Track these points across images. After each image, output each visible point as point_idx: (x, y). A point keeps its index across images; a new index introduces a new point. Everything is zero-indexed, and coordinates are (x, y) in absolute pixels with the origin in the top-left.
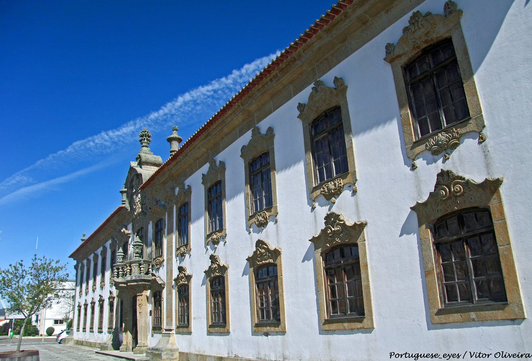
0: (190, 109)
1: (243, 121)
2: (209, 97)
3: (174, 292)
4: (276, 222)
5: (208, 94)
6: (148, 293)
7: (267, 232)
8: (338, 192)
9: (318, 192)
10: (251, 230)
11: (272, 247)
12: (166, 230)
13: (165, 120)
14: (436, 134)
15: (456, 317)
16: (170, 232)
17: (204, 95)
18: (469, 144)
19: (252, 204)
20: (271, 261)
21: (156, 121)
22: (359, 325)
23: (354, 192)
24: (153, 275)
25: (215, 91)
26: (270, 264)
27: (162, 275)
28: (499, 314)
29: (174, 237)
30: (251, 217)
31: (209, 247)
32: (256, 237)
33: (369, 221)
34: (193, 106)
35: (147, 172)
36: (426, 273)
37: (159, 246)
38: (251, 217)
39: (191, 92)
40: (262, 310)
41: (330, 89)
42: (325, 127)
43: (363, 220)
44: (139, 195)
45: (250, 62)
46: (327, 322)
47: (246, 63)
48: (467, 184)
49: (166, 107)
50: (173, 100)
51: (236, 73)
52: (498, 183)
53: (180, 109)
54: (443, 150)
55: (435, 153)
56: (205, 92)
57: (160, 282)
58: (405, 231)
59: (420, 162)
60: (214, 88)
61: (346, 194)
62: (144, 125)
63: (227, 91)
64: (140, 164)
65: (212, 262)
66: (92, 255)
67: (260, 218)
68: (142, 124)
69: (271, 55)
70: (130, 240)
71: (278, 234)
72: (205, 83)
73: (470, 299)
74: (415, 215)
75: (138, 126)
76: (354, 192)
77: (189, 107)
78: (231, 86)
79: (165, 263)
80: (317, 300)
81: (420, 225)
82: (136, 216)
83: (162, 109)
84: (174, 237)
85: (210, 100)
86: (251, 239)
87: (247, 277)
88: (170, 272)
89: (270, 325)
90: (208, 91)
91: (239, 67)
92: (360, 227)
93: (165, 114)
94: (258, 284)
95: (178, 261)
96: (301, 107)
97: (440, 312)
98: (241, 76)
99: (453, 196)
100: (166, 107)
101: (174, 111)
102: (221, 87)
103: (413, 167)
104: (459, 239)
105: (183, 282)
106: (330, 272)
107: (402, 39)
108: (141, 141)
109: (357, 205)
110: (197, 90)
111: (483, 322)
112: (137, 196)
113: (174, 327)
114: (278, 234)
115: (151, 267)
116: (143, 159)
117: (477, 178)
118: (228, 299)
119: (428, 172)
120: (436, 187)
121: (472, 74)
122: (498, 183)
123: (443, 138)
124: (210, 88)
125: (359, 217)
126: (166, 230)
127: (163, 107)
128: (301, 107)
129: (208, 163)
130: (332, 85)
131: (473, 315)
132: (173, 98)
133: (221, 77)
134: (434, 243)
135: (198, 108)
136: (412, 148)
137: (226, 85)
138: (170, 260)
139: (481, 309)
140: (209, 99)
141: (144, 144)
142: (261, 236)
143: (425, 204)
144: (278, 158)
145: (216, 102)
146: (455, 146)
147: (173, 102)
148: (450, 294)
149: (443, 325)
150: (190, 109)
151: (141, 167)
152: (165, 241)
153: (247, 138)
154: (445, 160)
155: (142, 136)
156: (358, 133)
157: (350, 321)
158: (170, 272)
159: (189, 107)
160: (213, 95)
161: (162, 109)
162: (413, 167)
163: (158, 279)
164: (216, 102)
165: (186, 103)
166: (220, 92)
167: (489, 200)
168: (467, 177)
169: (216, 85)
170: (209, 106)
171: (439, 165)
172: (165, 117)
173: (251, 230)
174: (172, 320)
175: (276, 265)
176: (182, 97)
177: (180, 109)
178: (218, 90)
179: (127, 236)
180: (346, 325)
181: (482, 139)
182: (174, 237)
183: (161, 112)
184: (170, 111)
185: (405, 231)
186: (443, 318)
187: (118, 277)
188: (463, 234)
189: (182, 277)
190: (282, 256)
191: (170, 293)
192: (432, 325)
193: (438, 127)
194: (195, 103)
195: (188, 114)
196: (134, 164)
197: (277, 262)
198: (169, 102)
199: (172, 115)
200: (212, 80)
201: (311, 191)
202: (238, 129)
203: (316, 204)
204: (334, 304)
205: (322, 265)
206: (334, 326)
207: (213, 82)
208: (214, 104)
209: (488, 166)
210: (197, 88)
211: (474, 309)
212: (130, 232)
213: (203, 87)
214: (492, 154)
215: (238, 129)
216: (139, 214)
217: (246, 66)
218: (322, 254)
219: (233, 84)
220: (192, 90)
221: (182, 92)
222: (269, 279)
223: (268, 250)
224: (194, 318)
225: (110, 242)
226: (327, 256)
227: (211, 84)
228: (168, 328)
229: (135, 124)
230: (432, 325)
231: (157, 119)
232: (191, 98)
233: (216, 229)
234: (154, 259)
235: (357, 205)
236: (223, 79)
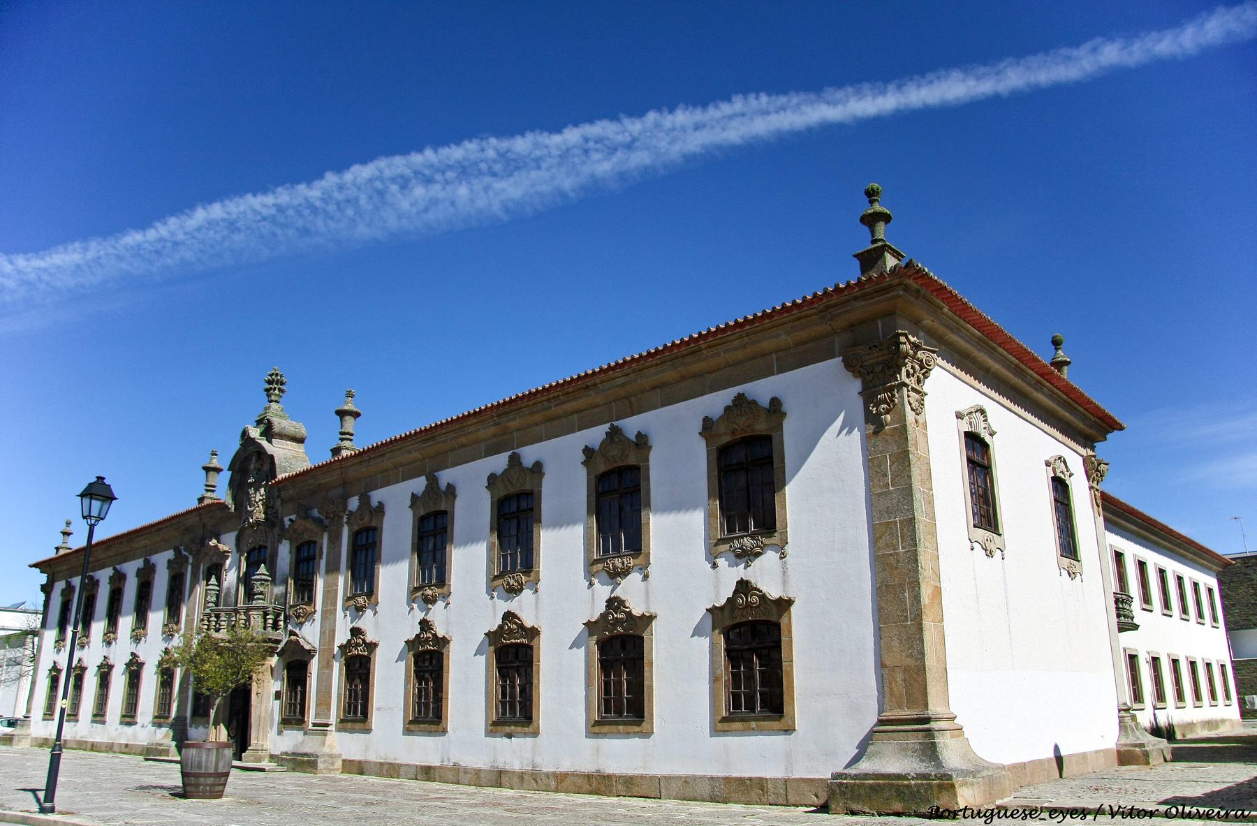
0: (218, 237)
1: (495, 436)
2: (264, 219)
3: (337, 668)
4: (536, 591)
5: (265, 212)
6: (274, 660)
7: (520, 601)
8: (625, 573)
9: (600, 566)
10: (495, 594)
11: (528, 623)
12: (323, 563)
13: (158, 252)
14: (742, 537)
15: (738, 725)
16: (333, 569)
17: (254, 211)
18: (770, 557)
19: (499, 559)
20: (525, 641)
21: (137, 250)
22: (637, 729)
23: (646, 577)
24: (292, 633)
25: (281, 209)
26: (522, 644)
27: (310, 634)
28: (775, 724)
29: (341, 580)
30: (496, 578)
31: (415, 606)
32: (503, 606)
33: (659, 613)
34: (225, 232)
35: (290, 459)
36: (714, 679)
37: (305, 588)
38: (496, 578)
39: (227, 202)
40: (503, 704)
41: (628, 440)
42: (616, 487)
43: (653, 611)
44: (262, 490)
45: (364, 161)
46: (597, 723)
47: (356, 163)
48: (763, 597)
49: (165, 224)
50: (183, 213)
51: (331, 179)
52: (789, 602)
53: (196, 234)
54: (746, 556)
55: (738, 556)
56: (258, 207)
57: (307, 647)
58: (697, 632)
59: (721, 562)
60: (279, 201)
61: (635, 577)
62: (107, 254)
63: (307, 212)
64: (269, 433)
65: (422, 629)
66: (109, 571)
67: (512, 582)
68: (102, 253)
69: (413, 154)
70: (228, 562)
71: (537, 608)
72: (260, 188)
73: (753, 709)
74: (710, 616)
75: (91, 255)
76: (646, 577)
77: (216, 232)
78: (318, 204)
79: (318, 616)
80: (587, 697)
81: (713, 629)
82: (251, 526)
83: (156, 229)
84: (342, 581)
85: (266, 227)
86: (494, 606)
87: (482, 659)
88: (328, 633)
89: (516, 724)
90: (264, 206)
91: (341, 168)
92: (648, 619)
93: (161, 240)
94: (500, 669)
95: (349, 618)
96: (588, 451)
97: (724, 720)
98: (341, 188)
99: (749, 606)
100: (165, 224)
101: (181, 237)
102: (295, 202)
103: (714, 566)
104: (749, 650)
105: (360, 651)
106: (606, 666)
107: (721, 417)
108: (267, 390)
109: (647, 593)
110: (241, 201)
111: (761, 731)
112: (257, 490)
113: (333, 719)
114: (537, 608)
115: (282, 617)
116: (276, 429)
117: (773, 592)
118: (651, 687)
119: (729, 575)
120: (734, 593)
121: (784, 485)
122: (789, 602)
123: (748, 544)
124: (269, 199)
125: (648, 607)
126: (323, 563)
127: (158, 224)
128: (588, 451)
129: (423, 478)
130: (632, 437)
131: (753, 724)
132: (183, 206)
133: (298, 183)
134: (726, 650)
135: (238, 238)
136: (716, 545)
137: (306, 199)
138: (329, 614)
139: (764, 719)
140: (266, 223)
141: (273, 398)
142: (514, 605)
143: (722, 608)
144: (548, 505)
145: (279, 231)
146: (758, 555)
147: (183, 218)
148: (735, 702)
149: (725, 733)
150: (218, 237)
151: (270, 442)
152: (320, 584)
153: (499, 462)
154: (746, 567)
155: (269, 382)
156: (656, 512)
157: (625, 724)
158: (328, 633)
159: (216, 232)
160: (274, 216)
161: (156, 229)
162: (714, 566)
163: (301, 641)
164: (279, 231)
165: (211, 224)
166: (291, 212)
167: (780, 616)
168: (764, 589)
169: (283, 196)
170: (261, 237)
171: (740, 572)
172: (159, 246)
173: (495, 594)
174: (329, 710)
175: (531, 648)
176: (205, 209)
177: (196, 234)
178: (289, 206)
179: (224, 556)
180: (621, 727)
181: (783, 556)
182: (341, 580)
183: (151, 234)
184: (172, 234)
185: (697, 632)
186: (726, 726)
187: (217, 630)
188: (754, 645)
189: (357, 645)
190: (542, 636)
191: (326, 666)
192: (715, 732)
193: (617, 548)
194: (232, 225)
195: (212, 246)
196: (255, 433)
197: (534, 643)
198: (172, 215)
199: (176, 244)
200: (277, 186)
201: (590, 563)
202: (483, 445)
203: (596, 581)
204: (607, 702)
205: (597, 655)
206: (606, 729)
207: (280, 189)
208: (274, 235)
209: (785, 583)
210: (241, 196)
211: (756, 719)
212: (226, 548)
213: (255, 195)
214: (790, 572)
215: (483, 445)
216: (258, 523)
217: (356, 168)
218: (597, 643)
219: (323, 200)
220: (231, 200)
221: (209, 198)
222: (517, 664)
223: (522, 626)
224: (378, 709)
225: (170, 554)
226: (603, 646)
227: (274, 193)
228: (319, 721)
229: (86, 250)
230: (715, 732)
231: (139, 246)
232: (225, 216)
233: (430, 580)
234: (291, 607)
235: (647, 593)
236: (302, 188)
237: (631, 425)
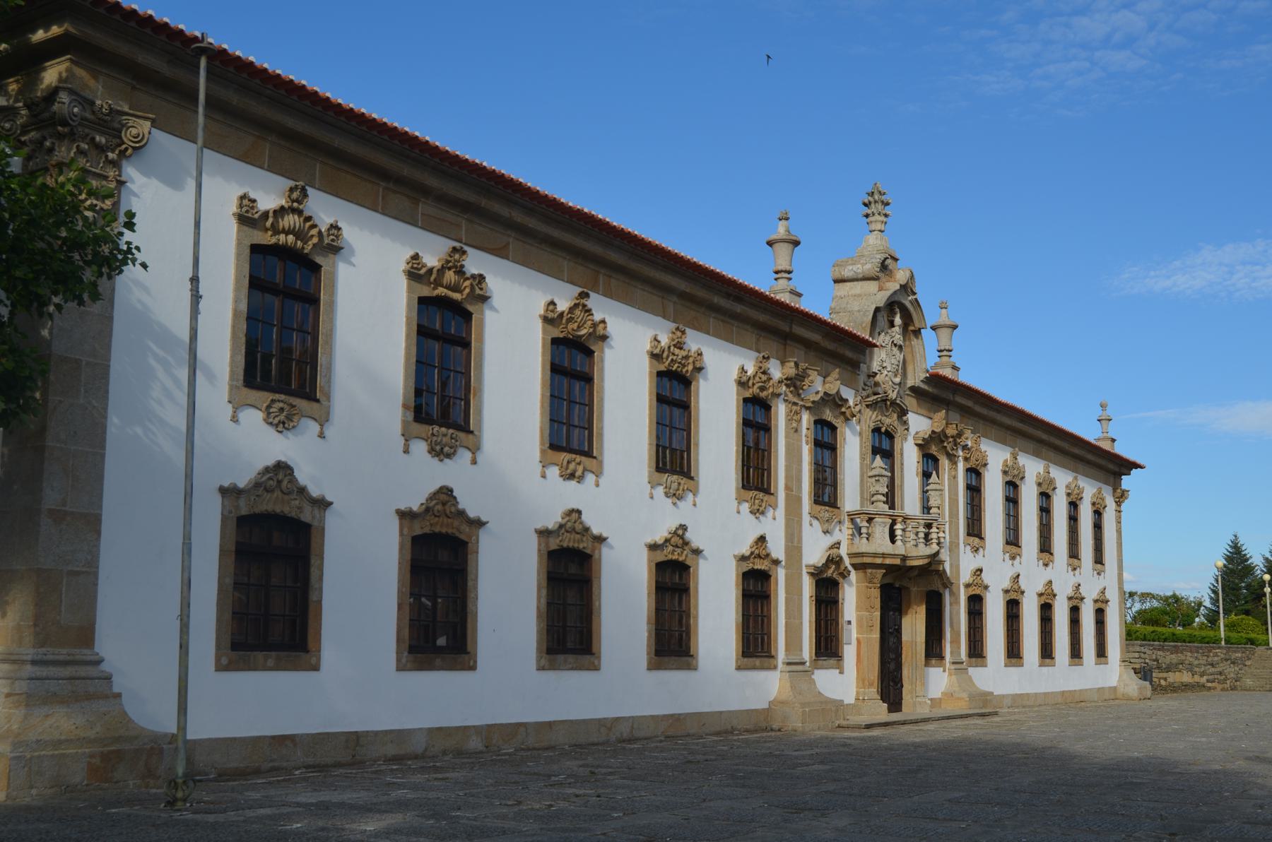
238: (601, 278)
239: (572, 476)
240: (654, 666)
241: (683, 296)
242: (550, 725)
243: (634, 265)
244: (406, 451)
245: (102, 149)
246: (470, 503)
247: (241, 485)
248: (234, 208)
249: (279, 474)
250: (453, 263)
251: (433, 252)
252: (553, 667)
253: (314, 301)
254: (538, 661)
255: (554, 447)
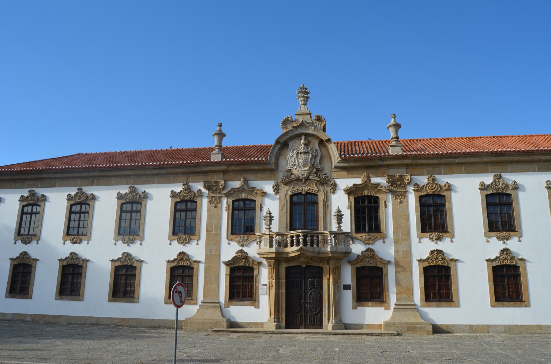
237: (443, 179)
238: (95, 181)
239: (75, 243)
240: (109, 301)
241: (239, 171)
242: (59, 316)
243: (102, 174)
244: (64, 244)
245: (400, 185)
246: (33, 255)
247: (68, 256)
248: (170, 194)
249: (127, 256)
250: (133, 190)
251: (125, 190)
252: (61, 299)
253: (511, 204)
254: (56, 296)
255: (232, 233)
